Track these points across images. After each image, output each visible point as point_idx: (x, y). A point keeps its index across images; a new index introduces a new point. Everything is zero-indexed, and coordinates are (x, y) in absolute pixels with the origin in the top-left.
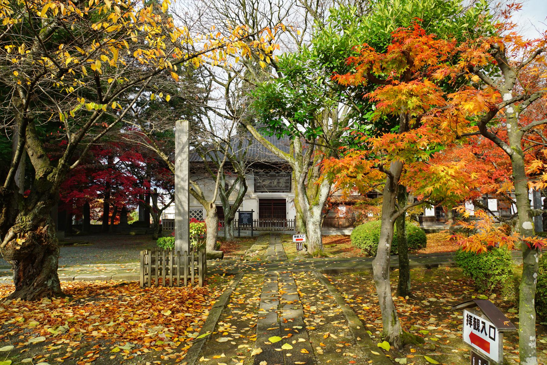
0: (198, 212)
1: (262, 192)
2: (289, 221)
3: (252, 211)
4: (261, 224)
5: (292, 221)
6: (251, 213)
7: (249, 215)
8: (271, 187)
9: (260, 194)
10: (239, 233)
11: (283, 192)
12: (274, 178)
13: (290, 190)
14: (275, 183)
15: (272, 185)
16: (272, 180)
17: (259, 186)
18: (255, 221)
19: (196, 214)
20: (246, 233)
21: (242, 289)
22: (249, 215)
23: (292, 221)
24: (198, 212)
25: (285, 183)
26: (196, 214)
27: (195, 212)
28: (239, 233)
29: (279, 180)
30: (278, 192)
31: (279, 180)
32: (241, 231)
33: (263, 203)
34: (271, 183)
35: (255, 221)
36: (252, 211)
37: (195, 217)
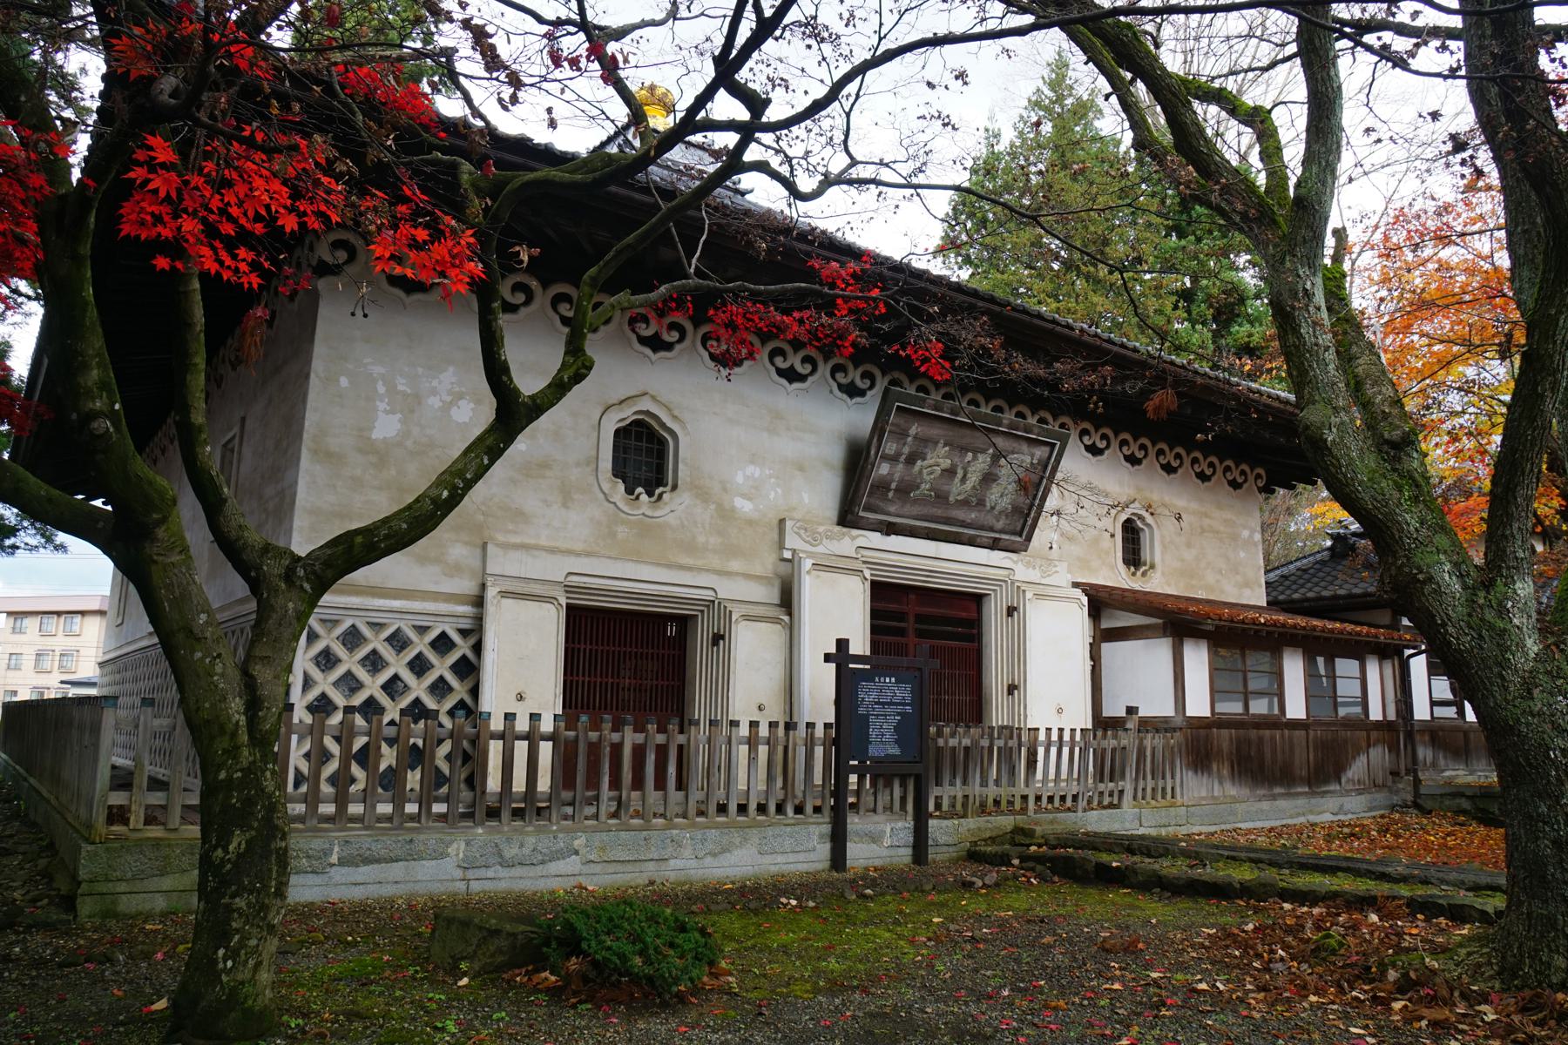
0: (421, 645)
1: (890, 529)
5: (532, 737)
10: (838, 839)
12: (979, 439)
19: (397, 665)
24: (421, 645)
26: (397, 665)
27: (398, 641)
28: (838, 839)
31: (998, 455)
32: (854, 822)
37: (393, 687)
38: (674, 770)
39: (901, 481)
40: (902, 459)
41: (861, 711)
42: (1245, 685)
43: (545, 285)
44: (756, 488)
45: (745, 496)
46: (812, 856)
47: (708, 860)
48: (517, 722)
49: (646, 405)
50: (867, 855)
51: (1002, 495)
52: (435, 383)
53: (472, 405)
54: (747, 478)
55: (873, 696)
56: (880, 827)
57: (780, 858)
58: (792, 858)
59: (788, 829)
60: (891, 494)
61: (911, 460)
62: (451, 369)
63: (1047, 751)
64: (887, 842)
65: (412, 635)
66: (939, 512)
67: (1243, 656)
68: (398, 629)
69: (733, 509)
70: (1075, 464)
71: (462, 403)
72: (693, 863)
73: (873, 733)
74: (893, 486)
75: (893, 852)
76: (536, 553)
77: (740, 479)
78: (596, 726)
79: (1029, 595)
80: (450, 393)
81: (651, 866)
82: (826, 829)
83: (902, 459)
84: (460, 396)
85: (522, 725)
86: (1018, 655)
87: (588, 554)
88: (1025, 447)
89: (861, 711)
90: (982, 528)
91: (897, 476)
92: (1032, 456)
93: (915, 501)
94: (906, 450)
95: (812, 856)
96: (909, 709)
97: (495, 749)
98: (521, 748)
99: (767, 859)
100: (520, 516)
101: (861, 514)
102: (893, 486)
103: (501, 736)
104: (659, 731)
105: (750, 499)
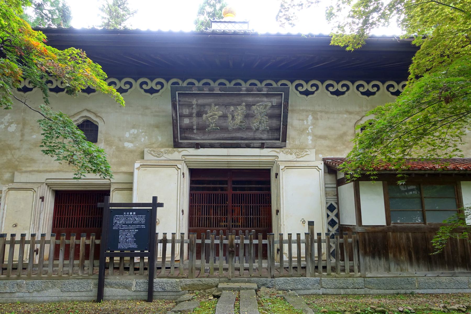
1: (198, 146)
2: (13, 243)
3: (155, 204)
4: (198, 250)
6: (150, 211)
7: (142, 219)
8: (224, 129)
9: (192, 151)
11: (262, 146)
12: (235, 100)
13: (284, 140)
14: (239, 118)
15: (231, 124)
16: (227, 105)
17: (189, 129)
18: (164, 241)
20: (127, 287)
21: (232, 245)
22: (142, 219)
23: (23, 242)
25: (271, 117)
29: (249, 106)
30: (248, 146)
31: (249, 106)
33: (202, 181)
34: (224, 116)
35: (164, 241)
36: (155, 204)
38: (263, 252)
39: (198, 124)
40: (194, 115)
41: (115, 228)
42: (422, 206)
43: (353, 83)
44: (135, 138)
45: (129, 141)
46: (90, 294)
47: (35, 294)
48: (26, 237)
49: (86, 114)
50: (122, 294)
51: (261, 121)
52: (3, 120)
53: (16, 125)
54: (130, 134)
55: (122, 221)
56: (129, 282)
57: (72, 294)
58: (79, 294)
59: (77, 281)
60: (195, 131)
61: (199, 115)
62: (9, 114)
63: (12, 247)
64: (133, 288)
65: (330, 219)
66: (226, 135)
67: (419, 190)
68: (331, 204)
69: (124, 147)
70: (295, 98)
71: (12, 125)
72: (27, 294)
73: (121, 238)
74: (195, 127)
75: (138, 294)
76: (33, 173)
77: (127, 135)
78: (68, 238)
79: (281, 167)
80: (8, 122)
81: (7, 295)
82: (96, 281)
83: (194, 115)
84: (12, 123)
85: (18, 238)
86: (278, 196)
87: (58, 171)
88: (265, 99)
89: (115, 228)
90: (255, 139)
91: (195, 123)
92: (271, 102)
93: (210, 132)
94: (195, 111)
95: (90, 294)
96: (143, 226)
97: (160, 246)
98: (17, 247)
99: (66, 294)
100: (32, 160)
101: (180, 141)
102: (195, 127)
103: (161, 241)
104: (340, 238)
105: (132, 142)
